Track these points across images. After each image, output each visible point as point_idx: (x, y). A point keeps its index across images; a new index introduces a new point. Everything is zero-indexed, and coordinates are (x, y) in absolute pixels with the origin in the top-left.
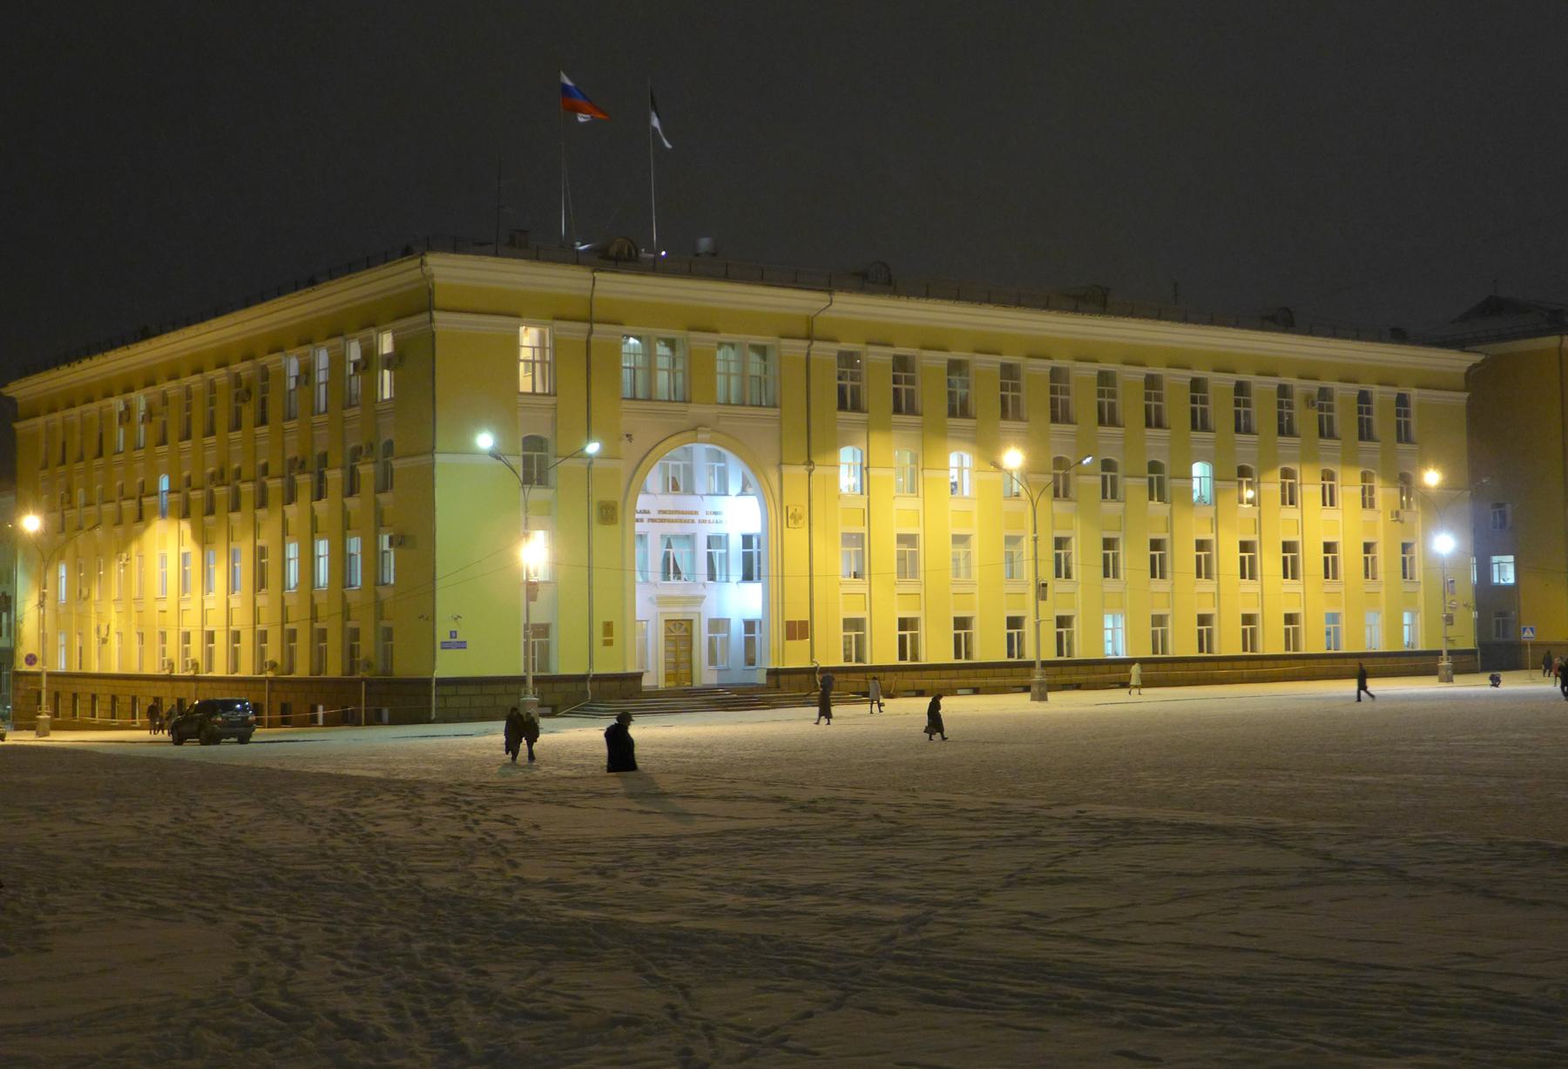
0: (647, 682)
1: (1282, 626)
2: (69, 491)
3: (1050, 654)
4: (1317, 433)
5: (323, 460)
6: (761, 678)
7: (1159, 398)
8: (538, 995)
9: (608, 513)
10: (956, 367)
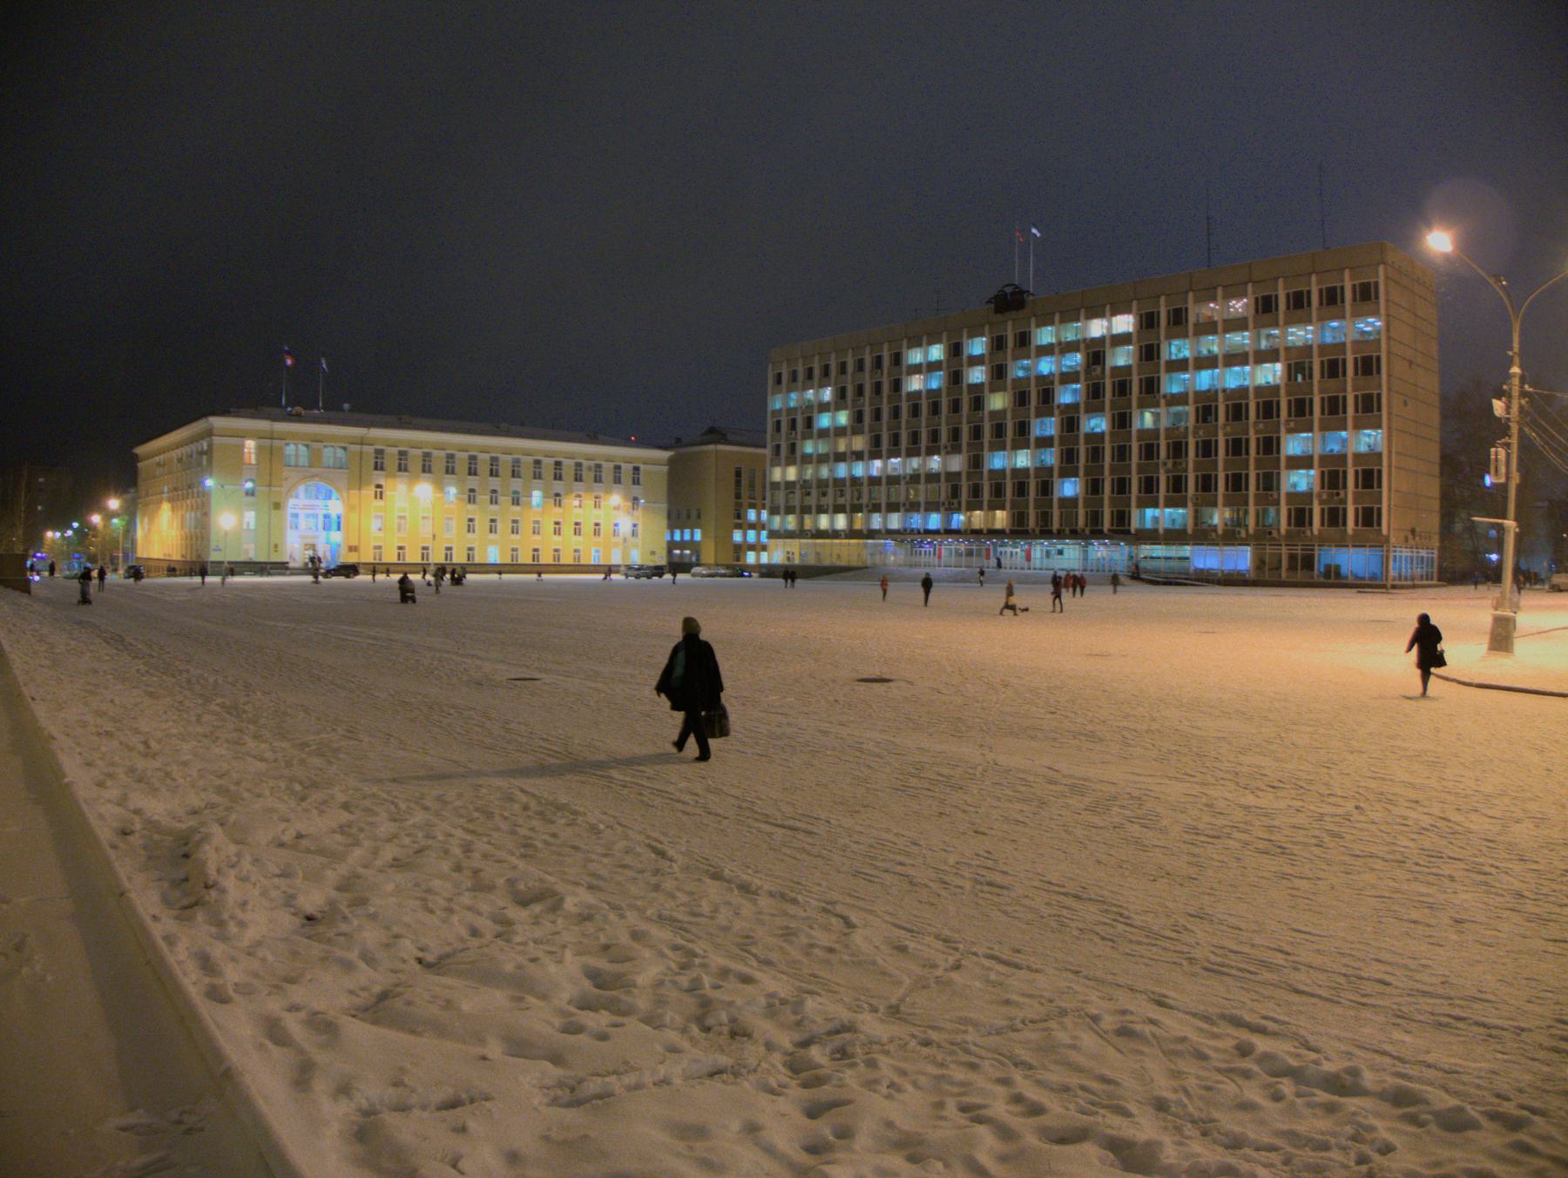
9: (277, 506)
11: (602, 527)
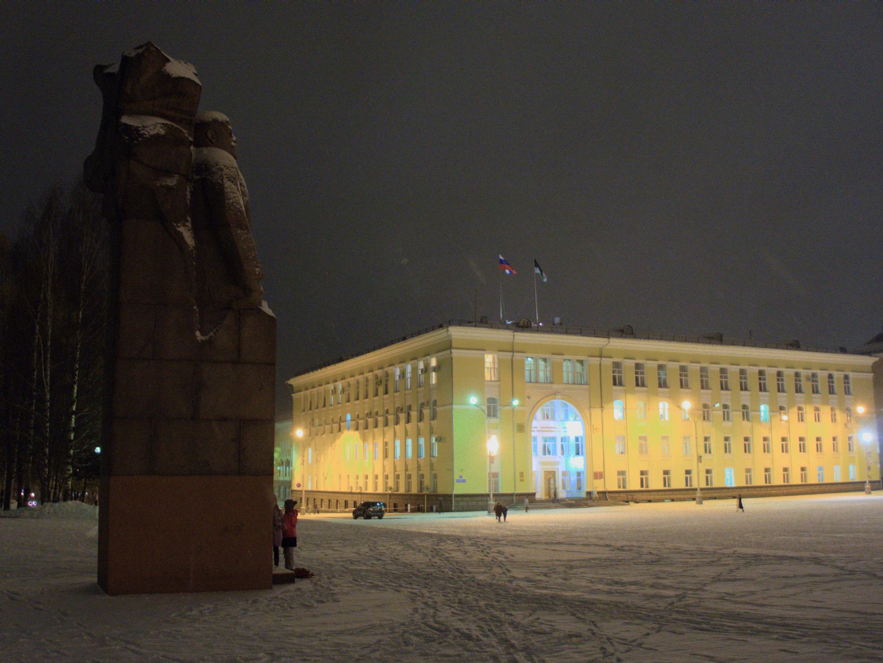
0: (538, 496)
1: (782, 472)
2: (313, 420)
3: (704, 485)
4: (739, 388)
5: (410, 407)
6: (584, 495)
7: (726, 377)
8: (536, 624)
9: (521, 428)
10: (661, 367)
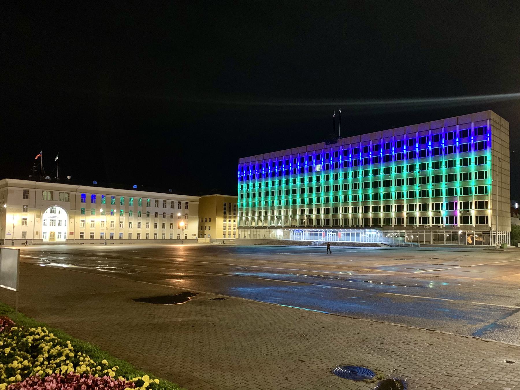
11: (28, 221)
